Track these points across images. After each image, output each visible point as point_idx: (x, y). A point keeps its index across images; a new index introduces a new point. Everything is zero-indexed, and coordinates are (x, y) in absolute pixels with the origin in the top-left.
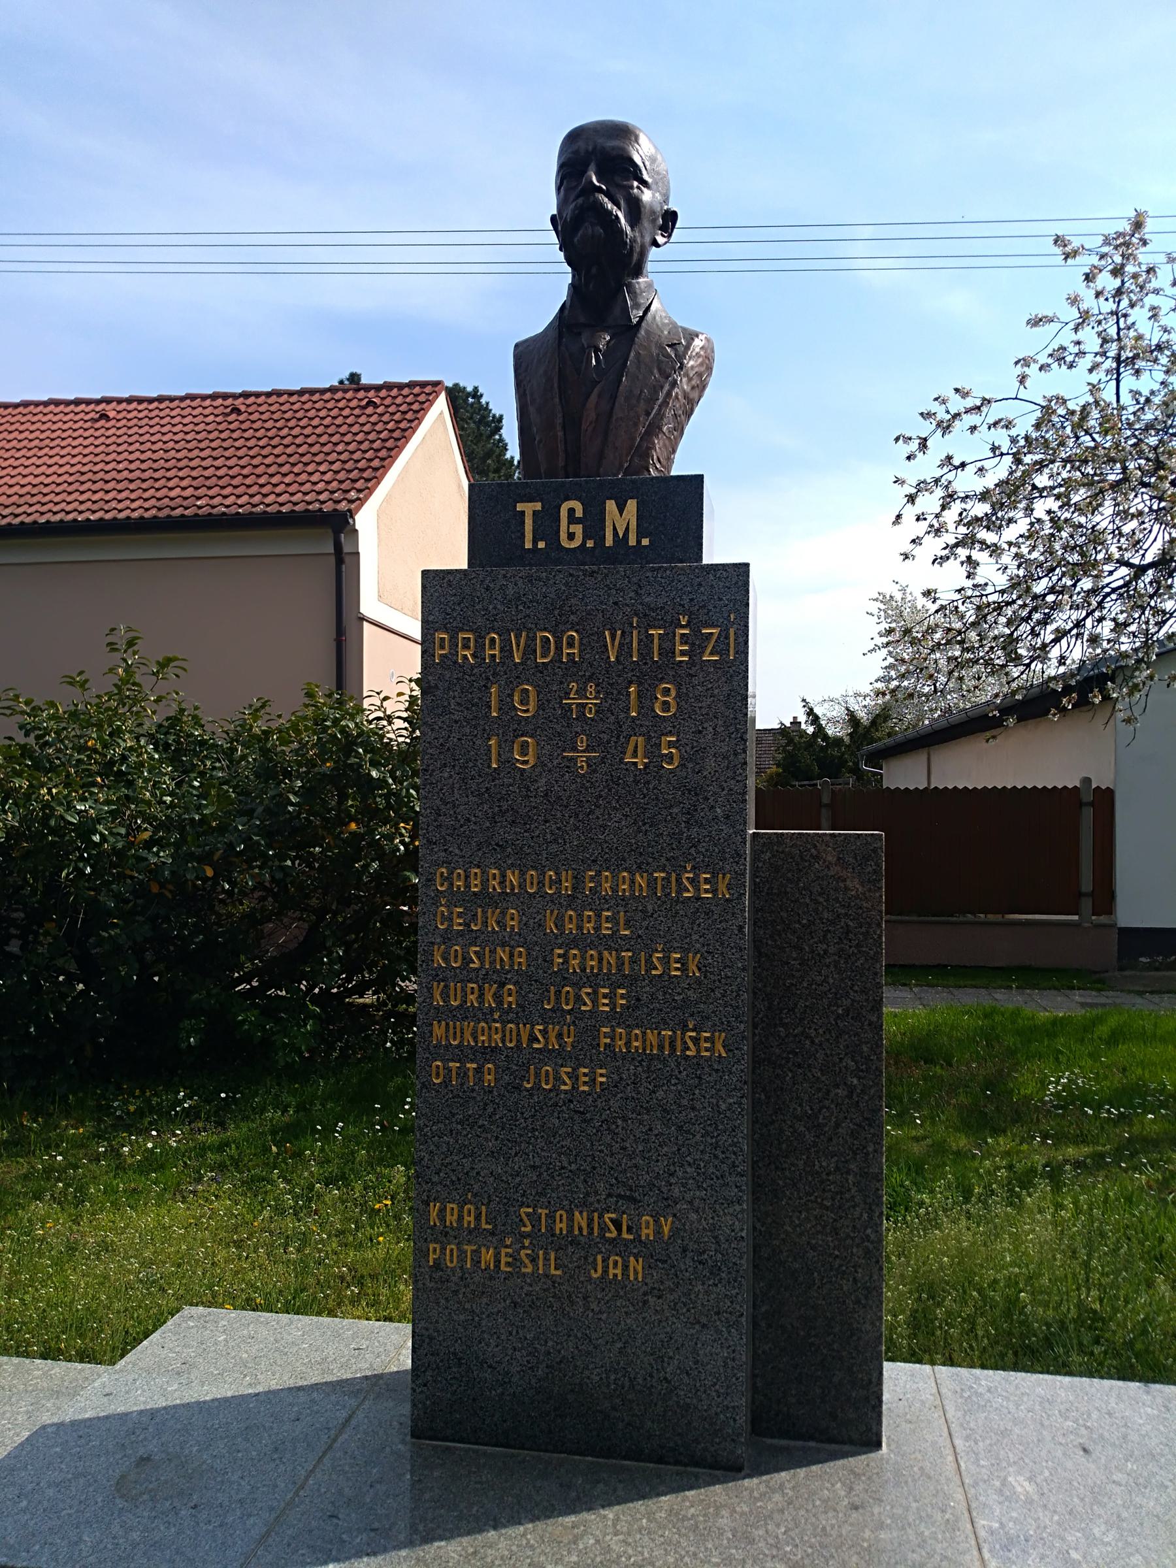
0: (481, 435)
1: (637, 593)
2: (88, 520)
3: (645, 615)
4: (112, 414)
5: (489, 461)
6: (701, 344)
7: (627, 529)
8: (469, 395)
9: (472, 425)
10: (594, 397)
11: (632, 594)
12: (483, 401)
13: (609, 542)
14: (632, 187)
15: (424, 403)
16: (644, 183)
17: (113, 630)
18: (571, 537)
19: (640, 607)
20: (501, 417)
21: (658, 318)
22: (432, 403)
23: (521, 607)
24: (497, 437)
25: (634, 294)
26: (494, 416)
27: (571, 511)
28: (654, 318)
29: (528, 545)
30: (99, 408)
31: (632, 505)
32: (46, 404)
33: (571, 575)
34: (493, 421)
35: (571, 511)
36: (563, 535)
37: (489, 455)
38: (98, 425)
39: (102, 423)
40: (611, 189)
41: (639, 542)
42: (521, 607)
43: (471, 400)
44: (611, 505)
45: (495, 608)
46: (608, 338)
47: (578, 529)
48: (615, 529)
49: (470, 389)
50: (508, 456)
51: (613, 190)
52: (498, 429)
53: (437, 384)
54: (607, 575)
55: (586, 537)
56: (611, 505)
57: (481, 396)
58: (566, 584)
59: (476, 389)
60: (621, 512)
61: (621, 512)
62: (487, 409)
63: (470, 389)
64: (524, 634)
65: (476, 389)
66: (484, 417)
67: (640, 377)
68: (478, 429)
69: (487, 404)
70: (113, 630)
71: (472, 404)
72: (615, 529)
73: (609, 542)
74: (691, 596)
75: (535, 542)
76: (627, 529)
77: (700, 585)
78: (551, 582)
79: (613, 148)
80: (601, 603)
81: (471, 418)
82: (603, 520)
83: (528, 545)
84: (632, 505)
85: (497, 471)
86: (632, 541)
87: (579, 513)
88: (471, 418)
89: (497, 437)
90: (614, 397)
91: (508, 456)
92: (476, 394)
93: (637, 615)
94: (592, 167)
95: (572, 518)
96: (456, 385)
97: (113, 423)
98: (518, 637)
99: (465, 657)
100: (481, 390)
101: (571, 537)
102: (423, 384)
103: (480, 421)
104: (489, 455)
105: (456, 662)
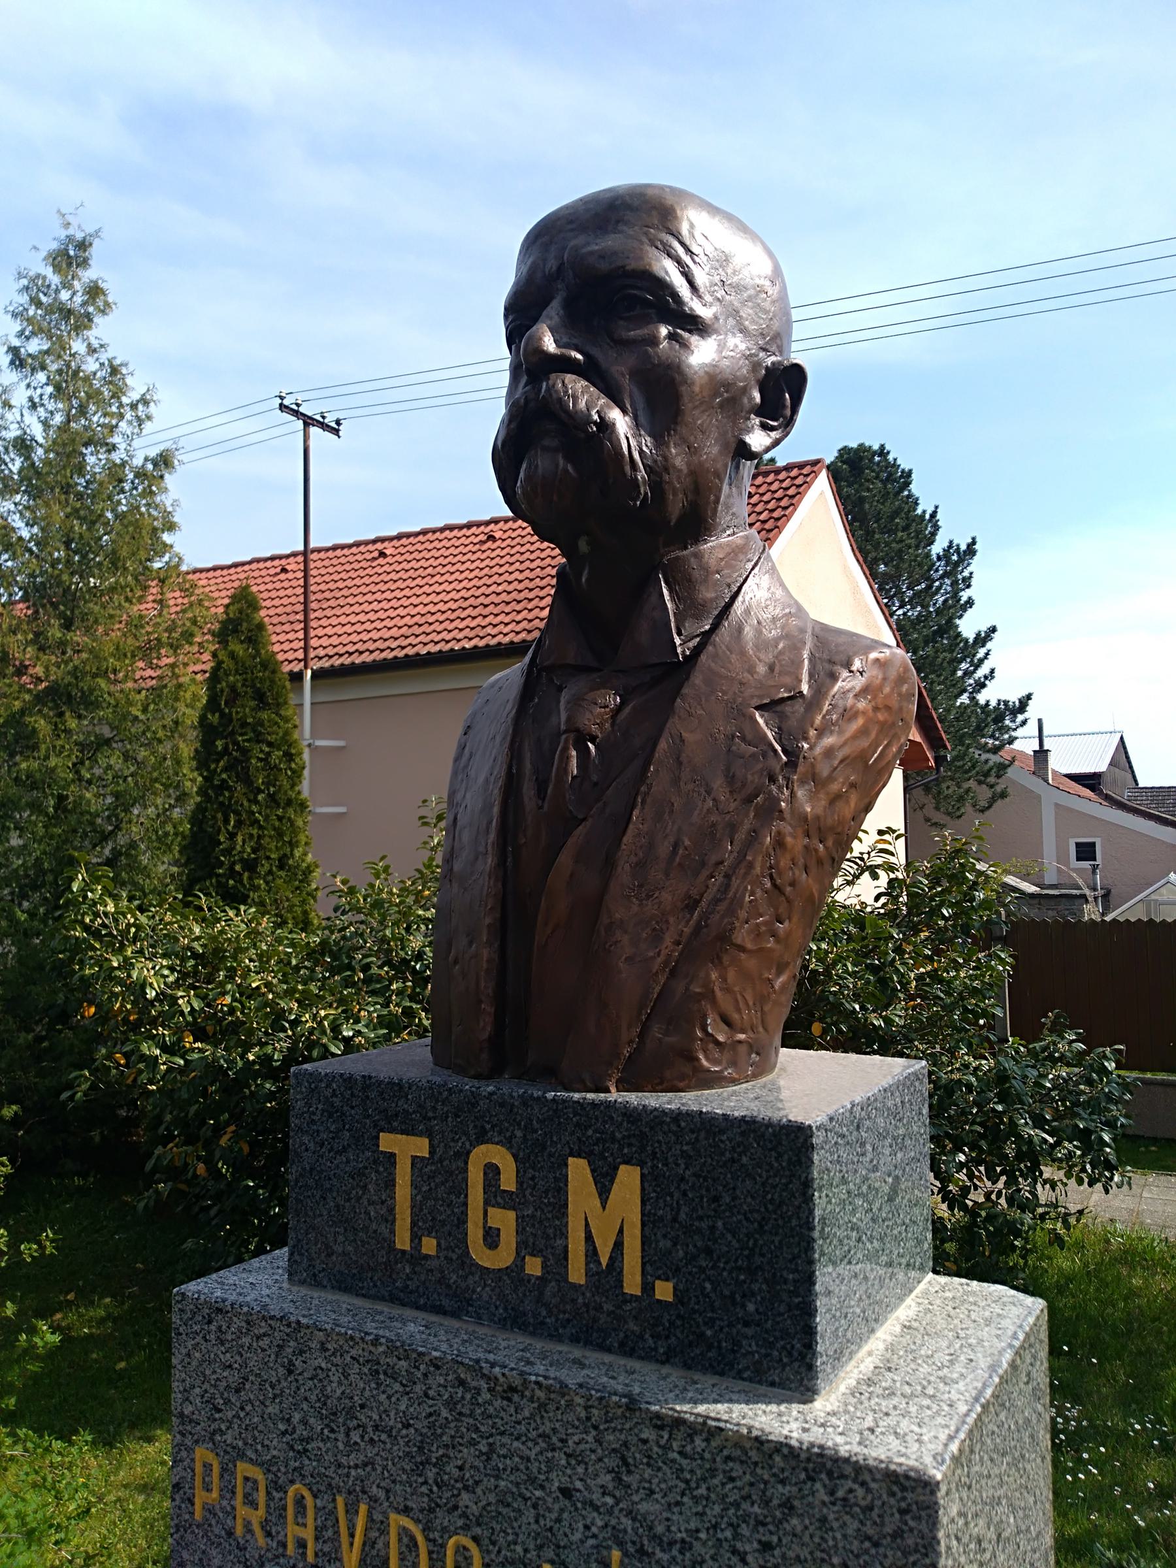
0: (888, 493)
1: (618, 1479)
2: (464, 648)
3: (642, 1552)
4: (497, 535)
5: (897, 520)
6: (858, 682)
7: (618, 1245)
8: (874, 453)
9: (880, 485)
10: (565, 859)
11: (606, 1479)
12: (891, 457)
13: (577, 1273)
14: (654, 341)
15: (801, 486)
16: (696, 325)
17: (425, 801)
18: (491, 1238)
19: (627, 1523)
20: (910, 471)
21: (749, 633)
22: (808, 485)
23: (355, 1437)
24: (906, 493)
25: (683, 584)
26: (903, 471)
27: (492, 1172)
28: (740, 629)
29: (403, 1241)
30: (487, 530)
31: (629, 1178)
32: (442, 530)
33: (462, 1383)
34: (901, 477)
35: (492, 1172)
36: (475, 1233)
37: (896, 513)
38: (484, 547)
39: (489, 544)
40: (595, 352)
41: (648, 1288)
42: (355, 1437)
43: (877, 459)
44: (578, 1170)
45: (304, 1421)
46: (614, 700)
47: (505, 1220)
48: (589, 1237)
49: (876, 447)
50: (919, 511)
51: (606, 357)
52: (907, 484)
53: (816, 463)
54: (542, 1406)
55: (524, 1247)
56: (578, 1170)
57: (888, 453)
58: (451, 1404)
59: (882, 447)
60: (604, 1192)
61: (604, 1192)
62: (895, 465)
63: (876, 447)
64: (363, 1508)
65: (882, 447)
66: (890, 474)
67: (677, 802)
68: (885, 487)
69: (895, 460)
70: (425, 801)
71: (879, 462)
72: (589, 1237)
73: (577, 1273)
74: (763, 1535)
75: (416, 1238)
76: (618, 1245)
77: (788, 1505)
78: (419, 1388)
79: (602, 256)
80: (532, 1480)
81: (877, 477)
82: (562, 1208)
83: (403, 1241)
84: (629, 1178)
85: (906, 528)
86: (632, 1284)
87: (508, 1182)
88: (877, 477)
89: (906, 493)
90: (609, 864)
91: (919, 511)
92: (882, 452)
93: (621, 1544)
94: (554, 309)
95: (494, 1195)
96: (861, 445)
97: (499, 543)
98: (351, 1510)
99: (247, 1525)
100: (888, 448)
101: (491, 1238)
102: (801, 466)
103: (888, 479)
104: (896, 513)
105: (230, 1534)
